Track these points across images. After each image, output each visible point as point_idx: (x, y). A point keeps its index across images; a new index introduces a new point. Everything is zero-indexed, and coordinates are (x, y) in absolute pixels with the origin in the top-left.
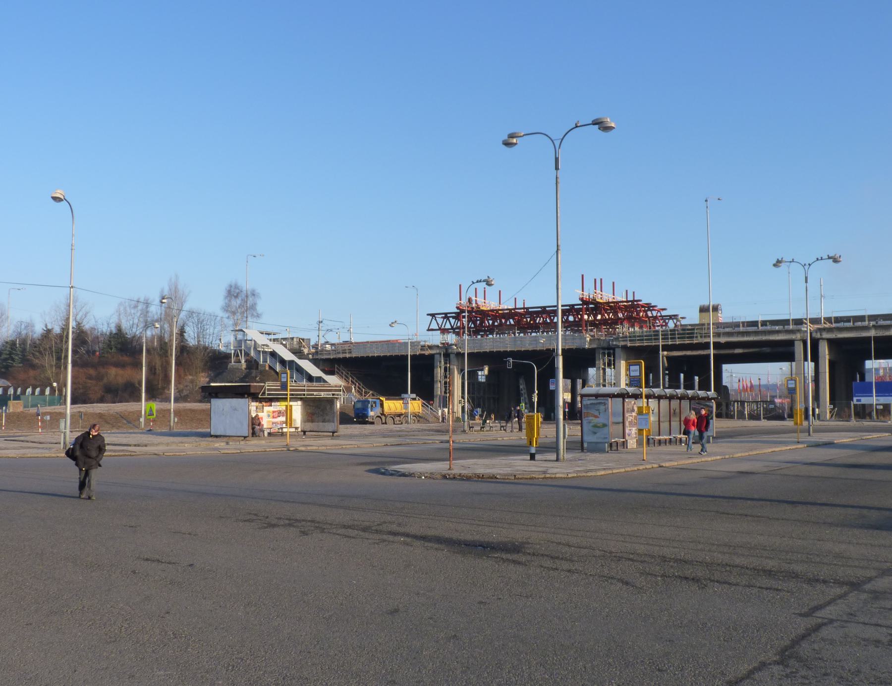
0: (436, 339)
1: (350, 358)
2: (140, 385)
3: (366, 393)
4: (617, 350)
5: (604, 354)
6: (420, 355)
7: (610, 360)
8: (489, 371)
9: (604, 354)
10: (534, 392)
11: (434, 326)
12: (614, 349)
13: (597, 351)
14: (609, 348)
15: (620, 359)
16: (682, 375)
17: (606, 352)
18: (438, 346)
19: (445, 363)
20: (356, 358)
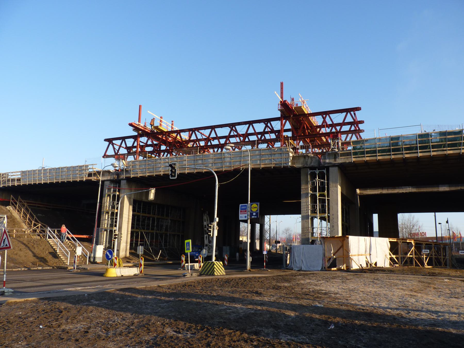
0: (110, 165)
1: (19, 186)
2: (246, 250)
3: (35, 225)
4: (331, 169)
5: (313, 176)
6: (87, 181)
7: (322, 183)
8: (357, 320)
9: (313, 176)
10: (212, 220)
11: (111, 152)
12: (328, 168)
13: (302, 172)
14: (320, 167)
15: (336, 182)
16: (375, 217)
17: (317, 172)
18: (109, 172)
19: (115, 191)
20: (24, 185)
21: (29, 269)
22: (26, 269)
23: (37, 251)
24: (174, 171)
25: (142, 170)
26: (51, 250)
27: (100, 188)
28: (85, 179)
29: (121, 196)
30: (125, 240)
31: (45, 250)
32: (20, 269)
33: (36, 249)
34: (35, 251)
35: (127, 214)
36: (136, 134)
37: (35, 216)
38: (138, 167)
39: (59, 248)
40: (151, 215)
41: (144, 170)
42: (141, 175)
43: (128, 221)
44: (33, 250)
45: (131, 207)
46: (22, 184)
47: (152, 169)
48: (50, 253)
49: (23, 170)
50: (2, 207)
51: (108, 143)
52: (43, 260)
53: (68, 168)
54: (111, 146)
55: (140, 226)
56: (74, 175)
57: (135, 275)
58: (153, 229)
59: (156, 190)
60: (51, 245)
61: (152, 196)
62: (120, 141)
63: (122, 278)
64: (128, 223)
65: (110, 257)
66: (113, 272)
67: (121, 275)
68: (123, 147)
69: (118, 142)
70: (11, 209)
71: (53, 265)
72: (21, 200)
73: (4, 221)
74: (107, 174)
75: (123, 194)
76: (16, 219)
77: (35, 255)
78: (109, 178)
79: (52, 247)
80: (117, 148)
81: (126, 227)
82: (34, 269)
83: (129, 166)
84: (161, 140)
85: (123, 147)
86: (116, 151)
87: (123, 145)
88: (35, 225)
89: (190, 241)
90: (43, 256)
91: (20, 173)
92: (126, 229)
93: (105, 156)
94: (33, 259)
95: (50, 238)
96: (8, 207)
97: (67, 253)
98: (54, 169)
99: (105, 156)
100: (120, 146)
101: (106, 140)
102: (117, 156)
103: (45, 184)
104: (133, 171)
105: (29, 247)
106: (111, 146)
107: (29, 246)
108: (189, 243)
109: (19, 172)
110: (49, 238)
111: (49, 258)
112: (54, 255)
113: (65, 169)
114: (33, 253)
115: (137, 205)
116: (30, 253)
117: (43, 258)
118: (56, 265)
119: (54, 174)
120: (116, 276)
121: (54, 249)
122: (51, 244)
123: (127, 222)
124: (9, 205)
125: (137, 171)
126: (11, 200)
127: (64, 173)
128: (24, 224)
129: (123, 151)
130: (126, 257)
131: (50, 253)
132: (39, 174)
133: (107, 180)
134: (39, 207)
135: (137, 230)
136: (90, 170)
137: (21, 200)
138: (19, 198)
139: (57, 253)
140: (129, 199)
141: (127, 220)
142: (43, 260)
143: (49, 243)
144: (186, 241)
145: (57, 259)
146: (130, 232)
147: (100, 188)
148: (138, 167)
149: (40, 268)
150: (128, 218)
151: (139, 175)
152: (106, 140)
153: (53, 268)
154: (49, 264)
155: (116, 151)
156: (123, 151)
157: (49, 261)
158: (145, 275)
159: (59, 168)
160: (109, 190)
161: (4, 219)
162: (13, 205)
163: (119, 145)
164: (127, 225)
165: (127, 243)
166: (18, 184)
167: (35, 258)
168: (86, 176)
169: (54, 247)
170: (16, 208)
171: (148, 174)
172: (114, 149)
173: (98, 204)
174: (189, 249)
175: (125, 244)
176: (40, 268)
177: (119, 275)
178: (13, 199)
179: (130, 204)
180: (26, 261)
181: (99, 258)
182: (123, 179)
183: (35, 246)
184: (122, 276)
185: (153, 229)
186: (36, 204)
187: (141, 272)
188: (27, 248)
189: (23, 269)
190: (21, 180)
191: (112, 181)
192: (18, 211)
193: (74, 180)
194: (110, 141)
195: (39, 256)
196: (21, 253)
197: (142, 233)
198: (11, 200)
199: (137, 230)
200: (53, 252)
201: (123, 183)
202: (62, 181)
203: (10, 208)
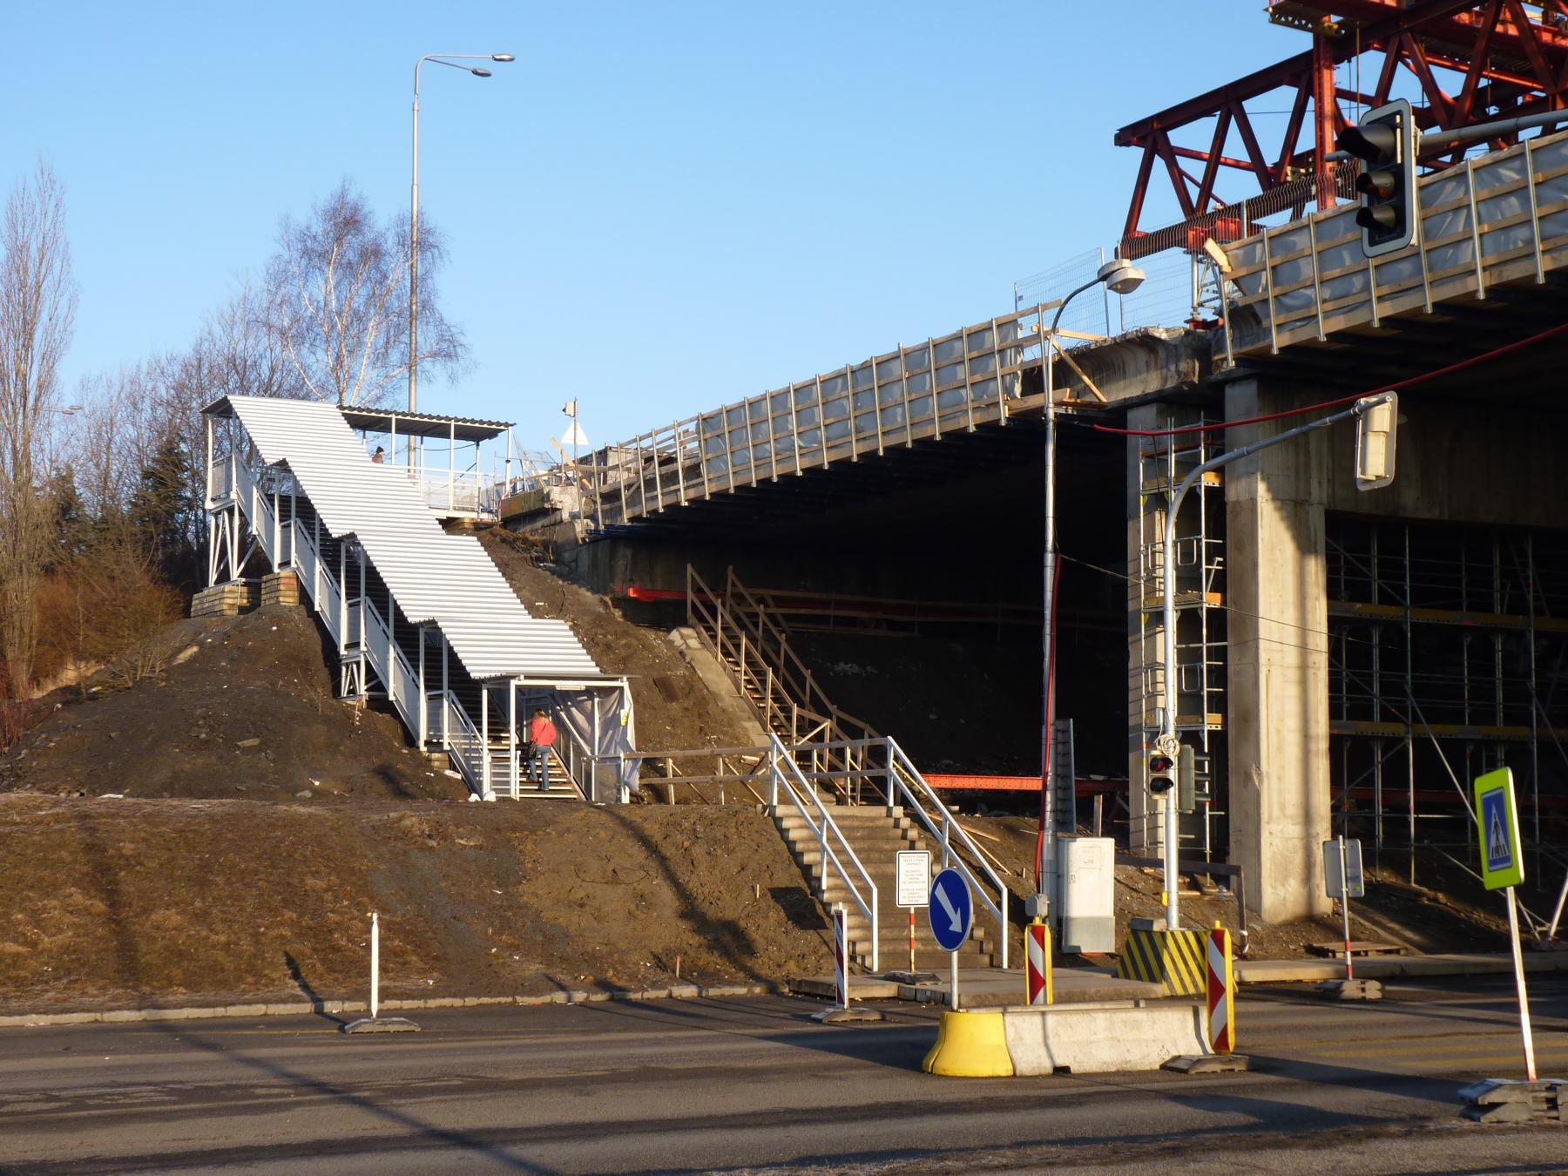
0: (1172, 296)
1: (697, 502)
19: (1188, 465)
21: (618, 996)
22: (600, 997)
23: (702, 882)
24: (1382, 181)
25: (1340, 287)
26: (786, 877)
27: (1050, 448)
28: (1004, 413)
29: (1233, 493)
30: (1293, 797)
31: (748, 874)
32: (560, 997)
33: (702, 869)
34: (692, 883)
35: (1291, 615)
36: (1299, 42)
37: (807, 673)
38: (1309, 269)
39: (831, 863)
40: (1498, 616)
41: (1358, 282)
42: (1339, 323)
43: (1304, 668)
44: (683, 878)
45: (1316, 569)
46: (707, 491)
47: (1406, 267)
48: (778, 894)
49: (708, 408)
50: (651, 636)
51: (1136, 154)
52: (727, 938)
53: (912, 357)
54: (1159, 164)
55: (1411, 701)
56: (948, 397)
57: (1171, 1067)
58: (1517, 717)
59: (1403, 408)
60: (791, 844)
61: (1376, 458)
62: (1208, 125)
63: (1061, 1088)
64: (1304, 683)
65: (956, 927)
66: (989, 1043)
67: (1047, 1067)
68: (1237, 165)
69: (1195, 135)
70: (694, 643)
71: (778, 975)
72: (741, 589)
73: (623, 713)
74: (1142, 356)
75: (1243, 483)
76: (715, 697)
77: (691, 912)
78: (1150, 383)
79: (796, 856)
80: (1196, 169)
81: (1292, 708)
82: (652, 994)
83: (1256, 274)
84: (1481, 44)
85: (1237, 165)
86: (1194, 193)
87: (1235, 147)
88: (805, 726)
89: (1506, 779)
90: (729, 914)
91: (692, 427)
92: (1292, 723)
93: (1136, 244)
94: (668, 930)
95: (785, 799)
96: (675, 635)
97: (866, 891)
98: (841, 375)
99: (1136, 244)
100: (1214, 160)
101: (1125, 137)
102: (1200, 223)
103: (813, 472)
104: (1282, 308)
105: (663, 860)
106: (1159, 164)
107: (668, 851)
108: (1496, 801)
109: (691, 420)
110: (780, 802)
111: (769, 929)
112: (803, 907)
113: (899, 369)
114: (682, 892)
115: (1353, 542)
116: (667, 895)
117: (731, 927)
118: (799, 975)
119: (849, 405)
120: (1004, 1070)
121: (806, 870)
122: (793, 835)
123: (1293, 675)
124: (685, 624)
125: (1310, 303)
126: (690, 596)
127: (896, 389)
128: (753, 727)
129: (1237, 187)
130: (1310, 919)
131: (778, 894)
132: (780, 419)
133: (1142, 401)
134: (851, 622)
135: (1391, 729)
136: (1030, 354)
137: (741, 589)
138: (731, 577)
139: (817, 891)
140: (1294, 510)
141: (1292, 657)
142: (730, 940)
143: (783, 832)
144: (1484, 784)
145: (811, 936)
146: (1322, 745)
147: (1050, 448)
148: (1309, 269)
149: (688, 991)
150: (1304, 649)
151: (1324, 329)
152: (1125, 137)
153: (772, 988)
154: (761, 965)
155: (1194, 193)
156: (1237, 187)
157: (760, 943)
158: (1259, 1065)
159: (866, 366)
160: (1156, 459)
161: (621, 704)
162: (702, 619)
163: (1206, 148)
164: (1293, 691)
165: (1307, 818)
166: (692, 494)
167: (683, 925)
168: (1008, 390)
169: (808, 858)
170: (714, 637)
171: (1379, 311)
172: (1178, 177)
173: (1049, 558)
174: (1502, 859)
175: (1294, 830)
176: (688, 991)
177: (1034, 1061)
178: (699, 591)
179: (1304, 547)
180: (622, 945)
181: (1094, 923)
182: (1231, 379)
183: (698, 851)
184: (1061, 1071)
185: (1517, 717)
186: (825, 604)
187: (1221, 1042)
188: (653, 865)
189: (579, 996)
190: (704, 469)
191: (1165, 401)
192: (726, 654)
193: (951, 426)
194: (1149, 136)
195: (712, 913)
196: (614, 900)
197: (1423, 745)
198: (690, 596)
199: (1391, 729)
200: (799, 890)
201: (1241, 400)
202: (894, 440)
203: (686, 638)
